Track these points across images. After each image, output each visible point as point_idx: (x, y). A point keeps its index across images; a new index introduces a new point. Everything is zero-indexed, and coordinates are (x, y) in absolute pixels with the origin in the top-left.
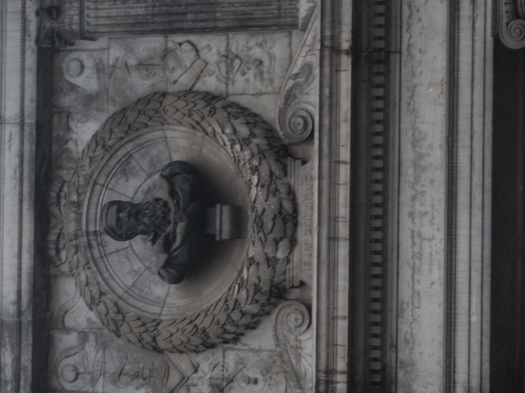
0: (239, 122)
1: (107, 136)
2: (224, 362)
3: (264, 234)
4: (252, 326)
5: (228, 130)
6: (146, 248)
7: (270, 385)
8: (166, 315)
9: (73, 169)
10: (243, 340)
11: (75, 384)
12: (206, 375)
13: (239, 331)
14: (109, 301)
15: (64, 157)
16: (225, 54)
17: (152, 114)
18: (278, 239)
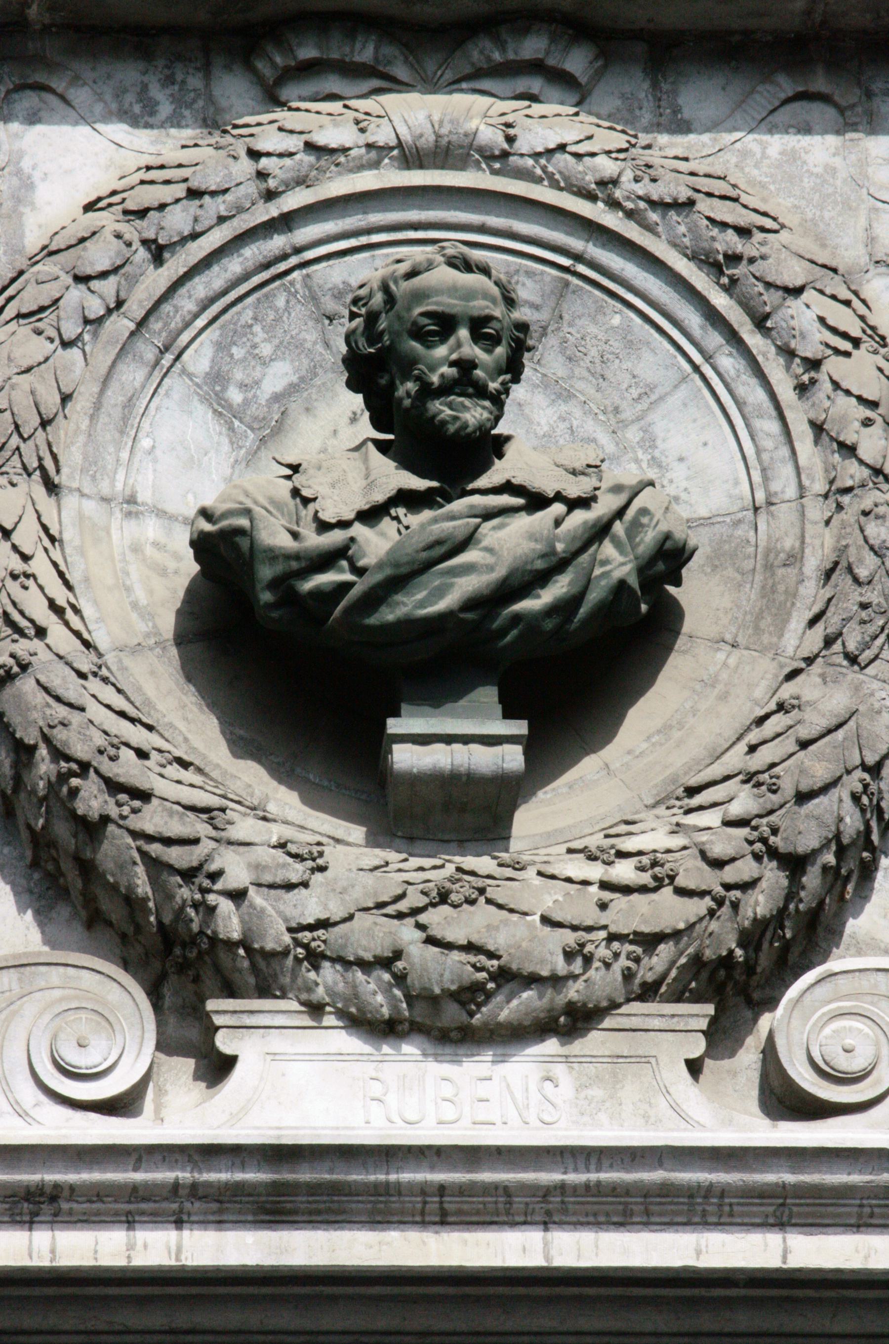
18: (400, 965)
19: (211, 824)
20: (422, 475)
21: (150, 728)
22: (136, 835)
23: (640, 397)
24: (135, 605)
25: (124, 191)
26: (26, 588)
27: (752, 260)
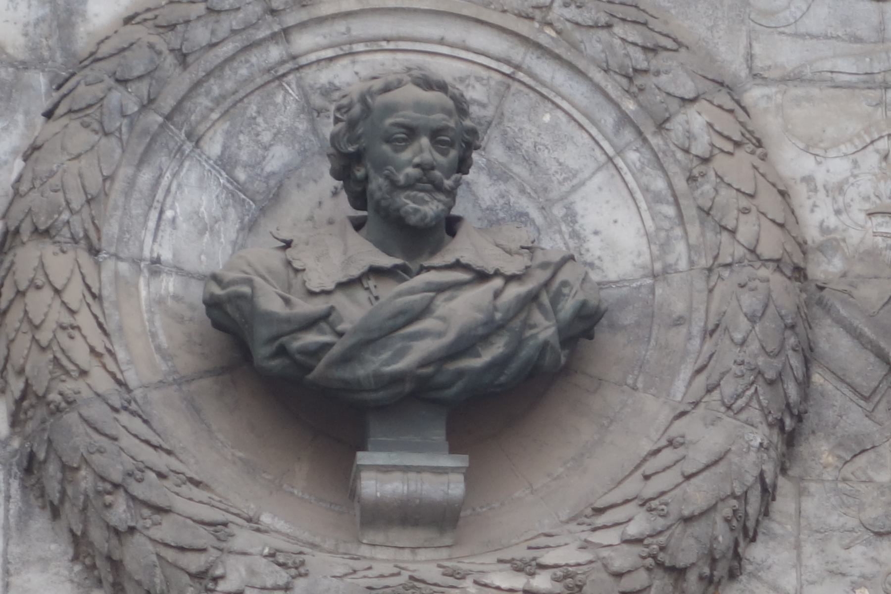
19: (216, 536)
20: (390, 254)
21: (169, 453)
22: (153, 541)
23: (565, 179)
24: (159, 349)
25: (156, 9)
26: (72, 337)
27: (657, 73)
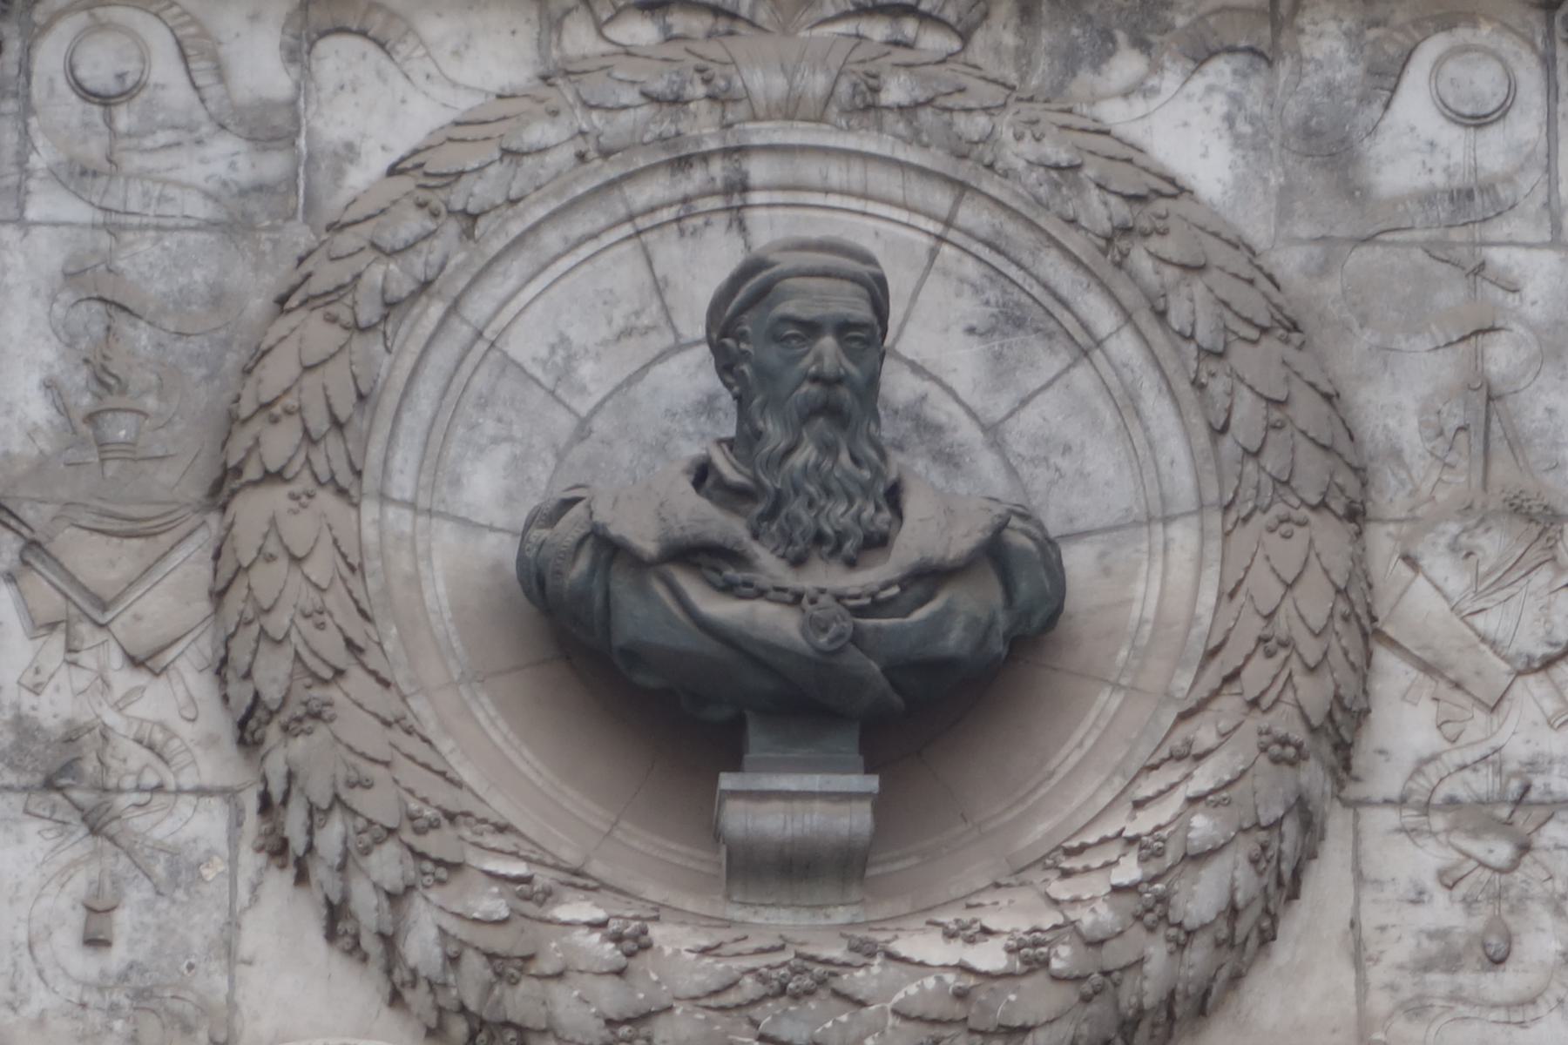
0: (1238, 874)
1: (1169, 247)
2: (179, 791)
3: (753, 1003)
4: (340, 927)
5: (1202, 825)
6: (671, 414)
7: (84, 1005)
8: (380, 523)
9: (1022, 79)
10: (280, 882)
11: (62, 86)
12: (119, 707)
13: (320, 873)
14: (435, 258)
15: (1075, 31)
16: (1533, 795)
17: (1273, 461)
